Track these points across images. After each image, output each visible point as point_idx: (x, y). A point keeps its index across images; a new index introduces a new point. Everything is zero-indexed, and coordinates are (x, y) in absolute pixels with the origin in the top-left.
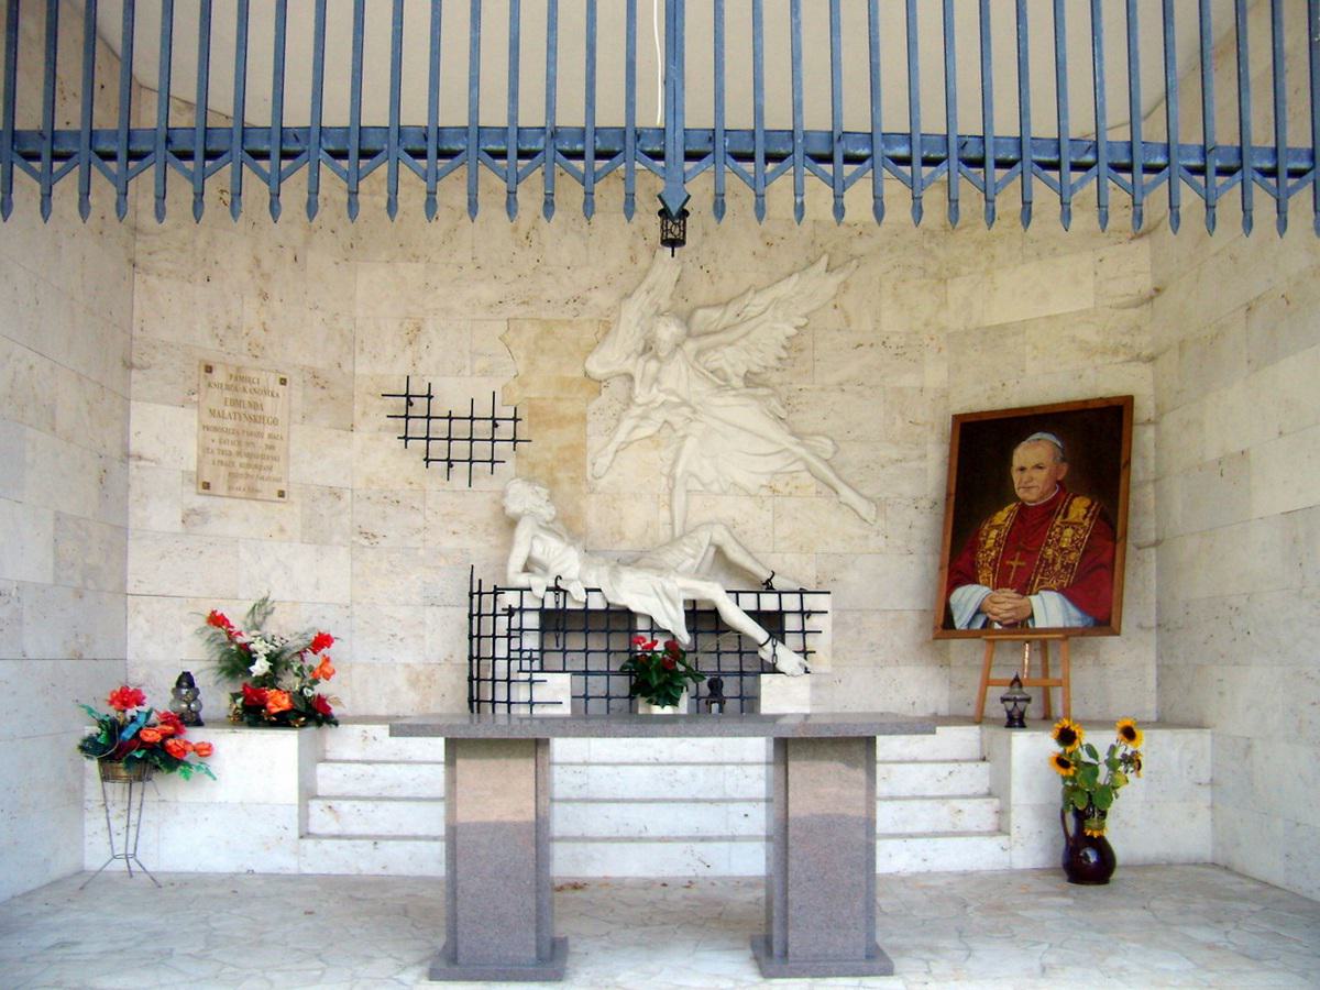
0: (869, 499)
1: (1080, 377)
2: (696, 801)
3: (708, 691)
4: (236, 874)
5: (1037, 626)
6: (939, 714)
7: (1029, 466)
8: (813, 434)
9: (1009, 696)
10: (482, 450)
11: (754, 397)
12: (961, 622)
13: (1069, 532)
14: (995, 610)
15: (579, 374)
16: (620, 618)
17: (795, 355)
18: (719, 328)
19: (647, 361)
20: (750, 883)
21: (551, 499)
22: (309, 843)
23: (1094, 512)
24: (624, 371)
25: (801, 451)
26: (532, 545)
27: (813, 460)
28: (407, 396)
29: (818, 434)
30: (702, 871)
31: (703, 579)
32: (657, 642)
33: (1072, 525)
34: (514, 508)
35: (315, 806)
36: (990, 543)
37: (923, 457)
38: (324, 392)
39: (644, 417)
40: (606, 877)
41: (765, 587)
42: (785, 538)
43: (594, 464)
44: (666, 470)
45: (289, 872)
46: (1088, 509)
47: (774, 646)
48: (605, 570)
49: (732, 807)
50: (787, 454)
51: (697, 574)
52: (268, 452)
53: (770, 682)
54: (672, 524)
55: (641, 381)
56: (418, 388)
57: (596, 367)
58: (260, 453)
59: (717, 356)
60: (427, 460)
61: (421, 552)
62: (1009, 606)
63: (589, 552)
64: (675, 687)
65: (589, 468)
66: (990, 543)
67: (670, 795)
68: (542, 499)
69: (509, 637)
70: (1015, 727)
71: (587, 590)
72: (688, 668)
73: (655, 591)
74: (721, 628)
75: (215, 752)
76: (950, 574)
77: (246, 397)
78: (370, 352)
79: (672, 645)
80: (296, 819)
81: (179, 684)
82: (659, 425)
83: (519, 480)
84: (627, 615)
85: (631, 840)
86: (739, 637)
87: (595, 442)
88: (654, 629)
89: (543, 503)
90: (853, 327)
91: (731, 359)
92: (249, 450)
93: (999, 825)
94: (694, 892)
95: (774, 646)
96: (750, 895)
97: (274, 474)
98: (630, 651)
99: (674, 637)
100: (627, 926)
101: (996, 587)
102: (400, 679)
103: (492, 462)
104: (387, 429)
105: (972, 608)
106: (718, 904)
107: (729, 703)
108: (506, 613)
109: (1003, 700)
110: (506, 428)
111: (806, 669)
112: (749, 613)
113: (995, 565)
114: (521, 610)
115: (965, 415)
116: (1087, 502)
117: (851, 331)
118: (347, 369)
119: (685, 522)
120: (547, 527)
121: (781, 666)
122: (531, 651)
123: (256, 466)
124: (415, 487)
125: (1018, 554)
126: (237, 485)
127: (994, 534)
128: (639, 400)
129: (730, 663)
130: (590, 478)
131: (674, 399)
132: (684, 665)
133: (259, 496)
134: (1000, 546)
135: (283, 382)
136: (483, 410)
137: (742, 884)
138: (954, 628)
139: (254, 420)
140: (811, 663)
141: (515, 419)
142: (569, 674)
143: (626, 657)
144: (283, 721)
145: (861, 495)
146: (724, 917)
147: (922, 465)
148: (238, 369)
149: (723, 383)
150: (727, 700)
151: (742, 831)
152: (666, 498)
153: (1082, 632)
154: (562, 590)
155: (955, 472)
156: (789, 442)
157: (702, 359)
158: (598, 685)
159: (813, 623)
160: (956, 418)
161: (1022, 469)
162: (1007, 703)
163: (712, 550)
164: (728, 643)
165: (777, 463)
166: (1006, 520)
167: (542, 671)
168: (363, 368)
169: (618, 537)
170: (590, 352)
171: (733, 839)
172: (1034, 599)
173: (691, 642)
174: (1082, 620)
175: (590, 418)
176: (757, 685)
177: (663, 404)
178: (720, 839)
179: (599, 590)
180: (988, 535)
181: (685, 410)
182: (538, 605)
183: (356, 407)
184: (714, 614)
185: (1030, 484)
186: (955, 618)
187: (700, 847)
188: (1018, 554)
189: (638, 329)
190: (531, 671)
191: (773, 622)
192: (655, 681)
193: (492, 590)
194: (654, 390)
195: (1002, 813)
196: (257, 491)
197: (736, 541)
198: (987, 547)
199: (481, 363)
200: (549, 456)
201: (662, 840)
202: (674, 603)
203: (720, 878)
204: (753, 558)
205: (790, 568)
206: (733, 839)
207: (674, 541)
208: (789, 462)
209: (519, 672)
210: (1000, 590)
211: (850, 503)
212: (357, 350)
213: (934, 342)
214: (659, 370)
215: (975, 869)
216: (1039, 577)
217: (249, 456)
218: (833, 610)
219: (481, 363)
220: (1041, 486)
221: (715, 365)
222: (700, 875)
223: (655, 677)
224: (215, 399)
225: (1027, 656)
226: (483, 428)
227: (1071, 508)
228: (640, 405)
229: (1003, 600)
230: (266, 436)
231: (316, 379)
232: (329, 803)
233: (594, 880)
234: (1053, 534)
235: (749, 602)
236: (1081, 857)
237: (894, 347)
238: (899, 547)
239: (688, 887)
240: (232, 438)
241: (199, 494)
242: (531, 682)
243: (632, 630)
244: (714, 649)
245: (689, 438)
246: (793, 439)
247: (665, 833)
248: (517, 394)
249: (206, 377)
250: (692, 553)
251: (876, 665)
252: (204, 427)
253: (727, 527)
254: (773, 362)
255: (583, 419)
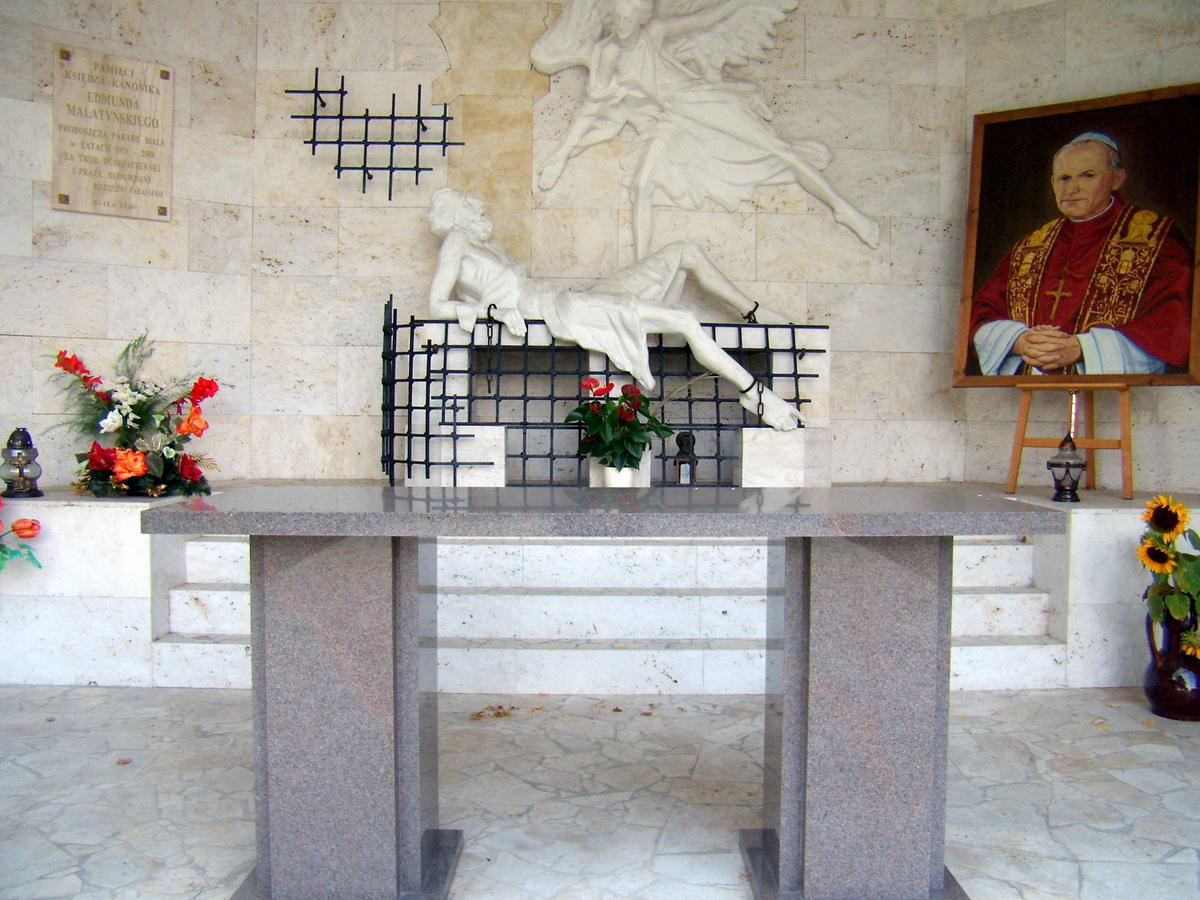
0: (873, 219)
1: (1139, 64)
2: (661, 592)
3: (677, 449)
4: (74, 687)
5: (1089, 371)
6: (953, 479)
7: (1074, 174)
8: (804, 139)
9: (1057, 461)
10: (405, 155)
11: (735, 92)
12: (988, 365)
13: (1128, 255)
14: (1033, 352)
15: (524, 66)
16: (569, 357)
17: (783, 45)
18: (692, 10)
19: (603, 47)
20: (733, 708)
21: (487, 214)
22: (165, 647)
23: (1163, 230)
24: (575, 62)
25: (789, 157)
26: (461, 268)
27: (802, 167)
28: (316, 92)
29: (810, 139)
30: (667, 688)
31: (672, 307)
32: (612, 385)
33: (1133, 246)
34: (440, 223)
35: (179, 598)
36: (1025, 269)
37: (935, 169)
38: (219, 90)
39: (601, 117)
40: (541, 695)
41: (747, 320)
42: (769, 264)
43: (540, 174)
44: (627, 181)
45: (139, 685)
46: (1155, 225)
47: (760, 393)
48: (550, 297)
49: (707, 601)
50: (772, 162)
51: (664, 302)
52: (145, 160)
53: (755, 438)
54: (634, 245)
55: (598, 70)
56: (328, 82)
57: (544, 57)
58: (135, 160)
59: (690, 44)
60: (339, 168)
61: (334, 281)
62: (1051, 347)
63: (532, 278)
64: (633, 443)
65: (535, 178)
66: (1025, 269)
67: (626, 584)
68: (475, 213)
69: (428, 380)
70: (1066, 500)
71: (528, 322)
72: (652, 419)
73: (612, 323)
74: (693, 369)
75: (41, 524)
76: (975, 305)
77: (117, 92)
78: (275, 44)
79: (632, 391)
80: (148, 617)
81: (11, 446)
82: (619, 127)
83: (448, 189)
84: (576, 354)
85: (575, 644)
86: (716, 380)
87: (542, 147)
88: (610, 370)
89: (477, 217)
90: (853, 12)
91: (710, 49)
92: (121, 157)
93: (1048, 627)
94: (656, 724)
95: (760, 393)
96: (728, 733)
97: (153, 186)
98: (578, 398)
99: (635, 380)
100: (557, 793)
101: (1035, 322)
102: (308, 435)
103: (417, 169)
104: (295, 134)
105: (1002, 349)
106: (689, 749)
107: (702, 465)
108: (424, 350)
109: (1051, 465)
110: (435, 128)
111: (799, 421)
112: (729, 351)
113: (1032, 298)
114: (446, 347)
115: (992, 115)
116: (1153, 217)
117: (850, 17)
118: (247, 62)
119: (650, 243)
120: (483, 247)
121: (767, 418)
122: (455, 398)
123: (130, 177)
124: (327, 202)
125: (1062, 282)
126: (105, 199)
127: (1029, 258)
128: (595, 94)
129: (704, 413)
130: (536, 190)
131: (638, 94)
132: (647, 415)
133: (134, 213)
134: (1038, 272)
135: (165, 75)
136: (406, 107)
137: (719, 710)
138: (981, 374)
139: (128, 120)
140: (805, 415)
141: (445, 118)
142: (502, 428)
143: (575, 404)
144: (135, 489)
145: (861, 212)
146: (696, 776)
147: (935, 178)
148: (106, 57)
149: (697, 77)
150: (700, 461)
151: (719, 634)
152: (627, 214)
153: (1150, 380)
154: (496, 322)
155: (978, 189)
156: (774, 145)
157: (671, 48)
158: (539, 440)
159: (807, 364)
160: (978, 118)
161: (1066, 178)
162: (1056, 469)
163: (683, 276)
164: (702, 388)
165: (760, 173)
166: (1044, 241)
167: (470, 423)
168: (267, 62)
169: (569, 262)
170: (538, 39)
171: (707, 644)
172: (1084, 339)
173: (656, 387)
174: (1149, 364)
175: (536, 118)
176: (739, 442)
177: (623, 100)
178: (692, 644)
179: (542, 322)
180: (1022, 257)
181: (651, 109)
182: (467, 341)
183: (258, 109)
184: (686, 351)
185: (1077, 196)
186: (982, 361)
187: (664, 656)
188: (1062, 282)
189: (595, 12)
190: (455, 424)
191: (757, 362)
192: (609, 436)
193: (408, 321)
194: (613, 83)
195: (1055, 613)
196: (131, 207)
197: (712, 264)
198: (1021, 273)
199: (407, 55)
200: (488, 164)
201: (615, 645)
202: (634, 338)
203: (690, 698)
204: (734, 287)
205: (778, 300)
206: (707, 644)
207: (637, 263)
208: (775, 171)
209: (440, 424)
210: (1038, 327)
211: (848, 222)
212: (260, 43)
213: (949, 33)
214: (619, 56)
215: (1020, 687)
216: (1090, 311)
217: (122, 164)
218: (831, 351)
219: (407, 55)
220: (1091, 199)
221: (687, 55)
222: (664, 692)
223: (609, 429)
224: (75, 92)
225: (1074, 410)
226: (407, 129)
227: (1132, 224)
228: (596, 101)
229: (1043, 339)
230: (142, 140)
231: (205, 71)
232: (194, 594)
233: (526, 700)
234: (1107, 257)
235: (728, 337)
236: (1174, 682)
237: (901, 36)
238: (906, 277)
239: (648, 714)
240: (98, 141)
241: (55, 209)
242: (455, 436)
243: (582, 372)
244: (684, 395)
245: (656, 141)
246: (782, 144)
247: (619, 635)
248: (448, 90)
249: (62, 65)
250: (658, 279)
251: (878, 418)
252: (60, 126)
253: (701, 249)
254: (758, 54)
255: (528, 119)
